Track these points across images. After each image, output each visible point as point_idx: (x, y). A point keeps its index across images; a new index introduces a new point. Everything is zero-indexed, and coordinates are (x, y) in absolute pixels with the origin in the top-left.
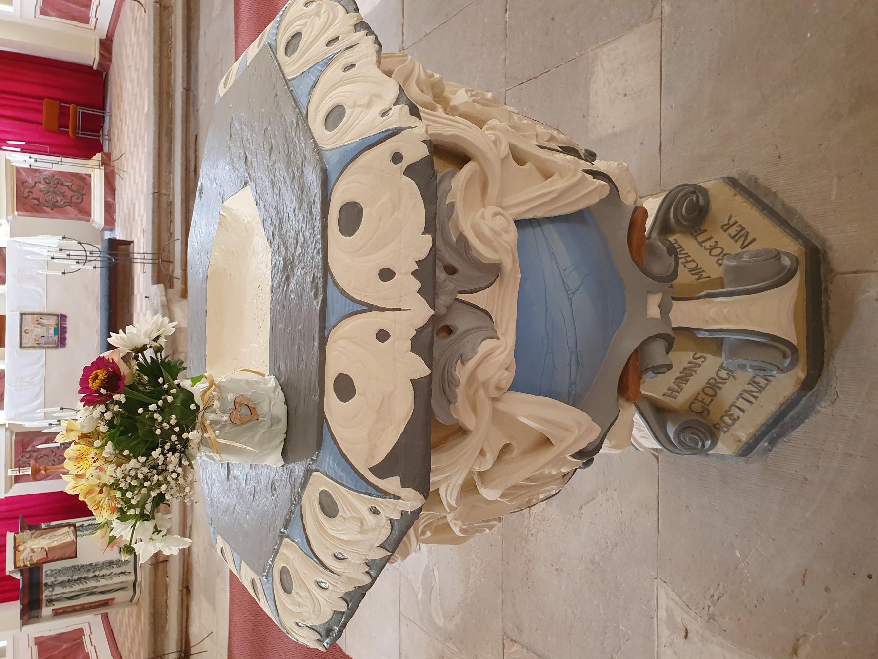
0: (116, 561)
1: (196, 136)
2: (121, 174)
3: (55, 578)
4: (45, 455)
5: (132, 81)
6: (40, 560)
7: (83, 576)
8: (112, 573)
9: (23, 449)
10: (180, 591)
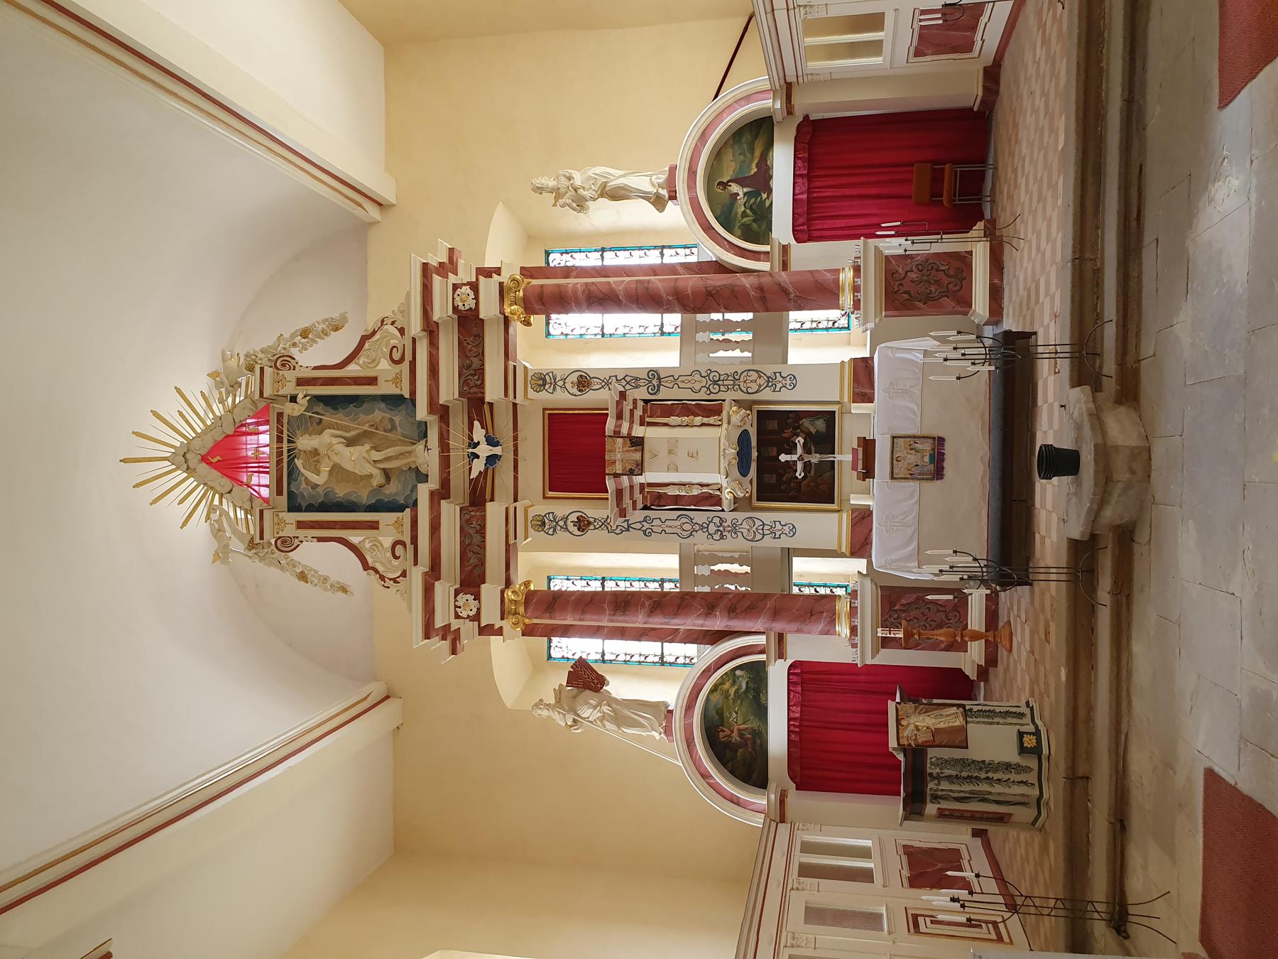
0: (1015, 764)
1: (1141, 166)
2: (1015, 242)
3: (941, 769)
4: (914, 618)
5: (1035, 111)
6: (926, 742)
7: (975, 775)
8: (1009, 779)
9: (891, 607)
10: (1111, 823)
